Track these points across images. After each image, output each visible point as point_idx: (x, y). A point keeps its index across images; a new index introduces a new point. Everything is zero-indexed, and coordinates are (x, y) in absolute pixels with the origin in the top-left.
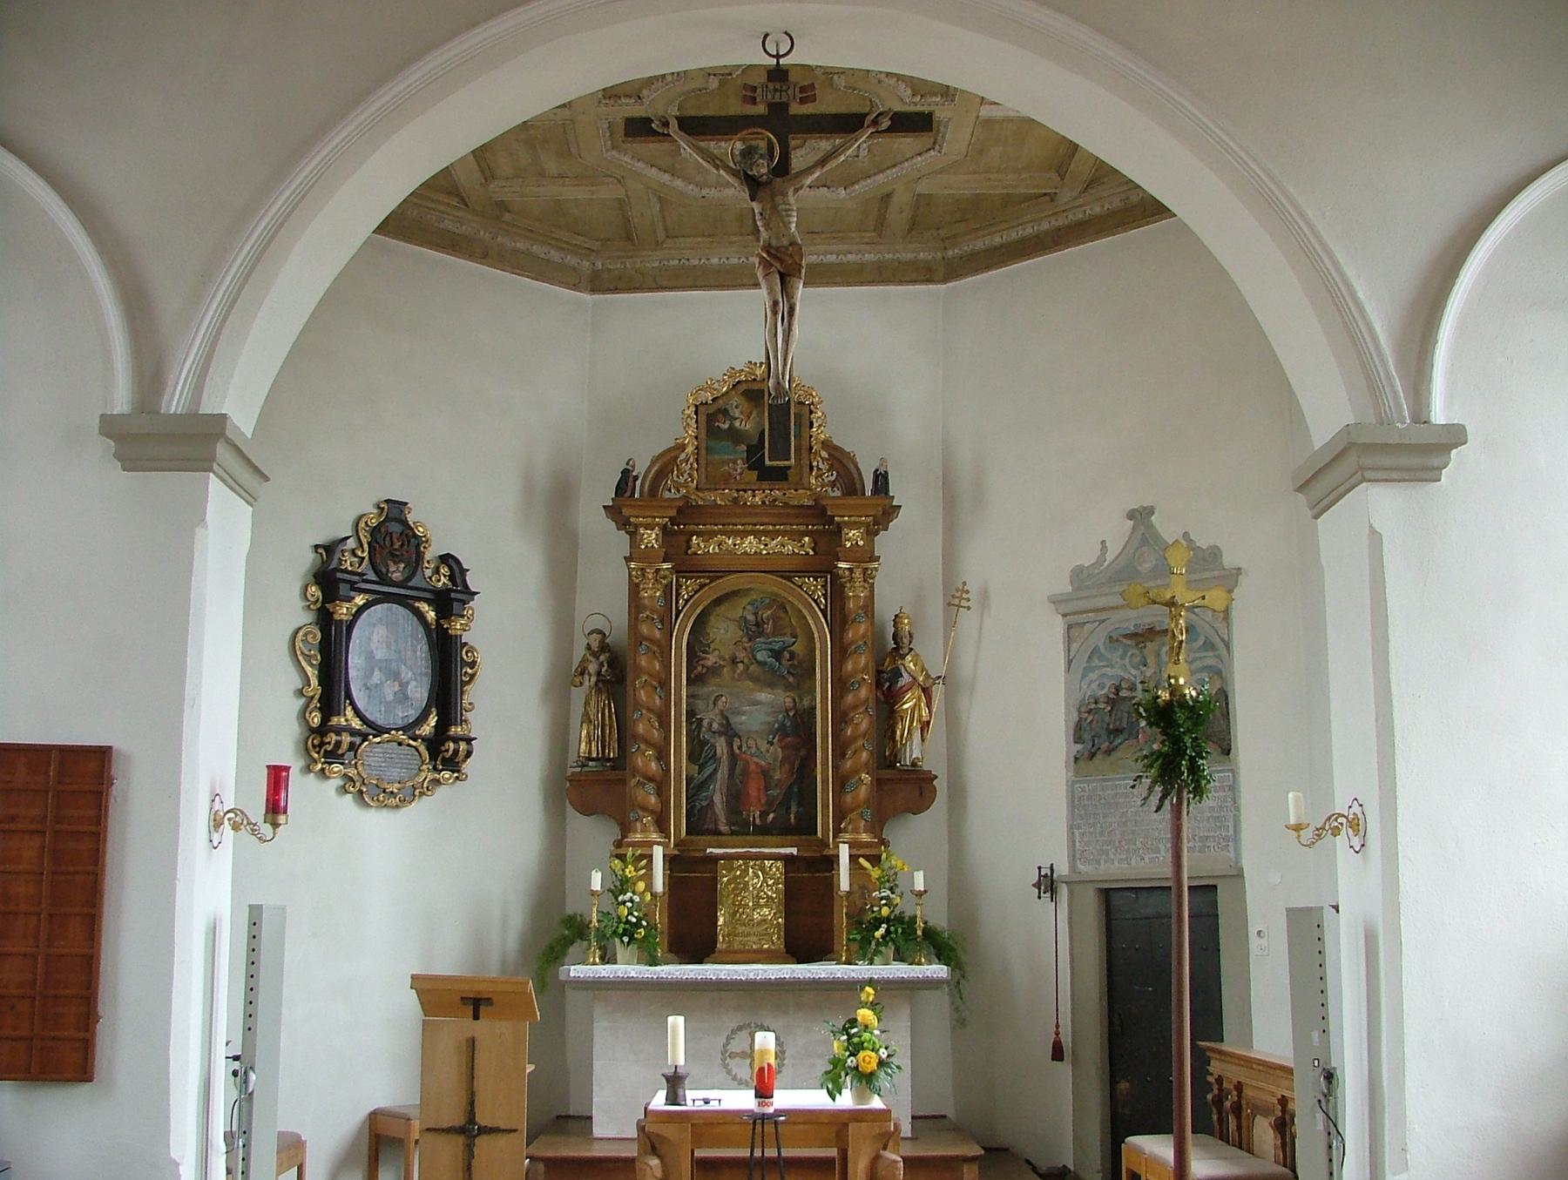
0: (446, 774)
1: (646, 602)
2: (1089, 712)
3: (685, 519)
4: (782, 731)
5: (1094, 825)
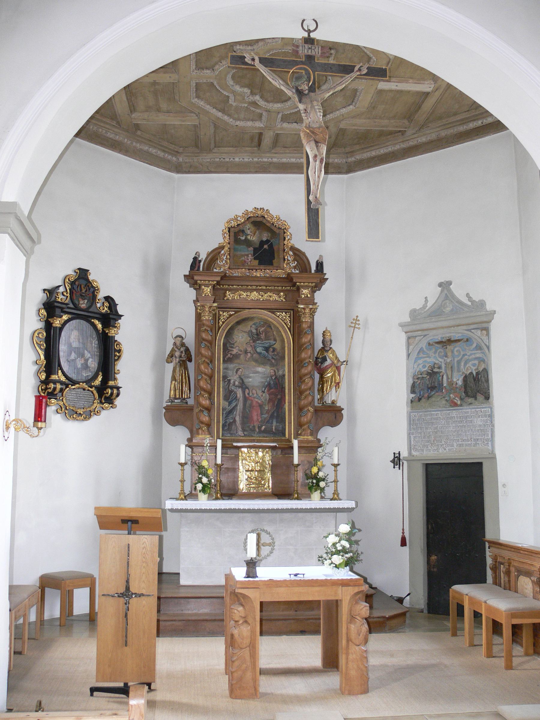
0: (106, 405)
1: (204, 322)
2: (418, 379)
3: (223, 284)
5: (421, 433)
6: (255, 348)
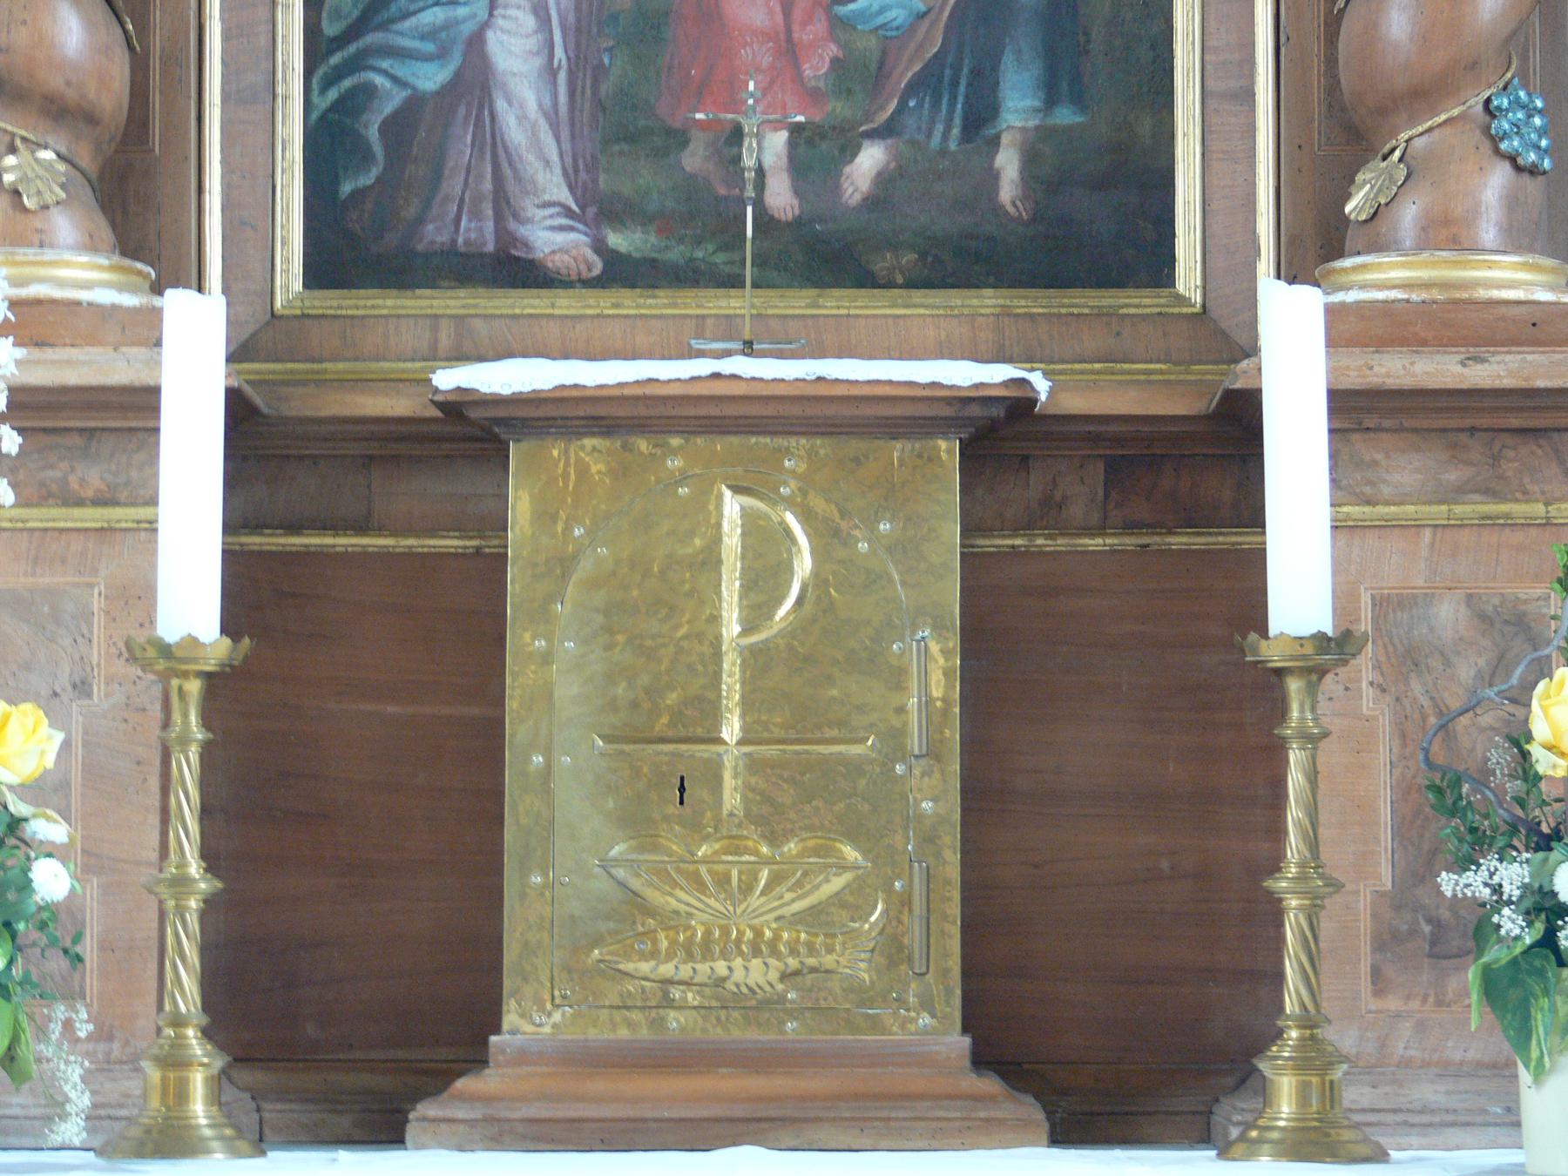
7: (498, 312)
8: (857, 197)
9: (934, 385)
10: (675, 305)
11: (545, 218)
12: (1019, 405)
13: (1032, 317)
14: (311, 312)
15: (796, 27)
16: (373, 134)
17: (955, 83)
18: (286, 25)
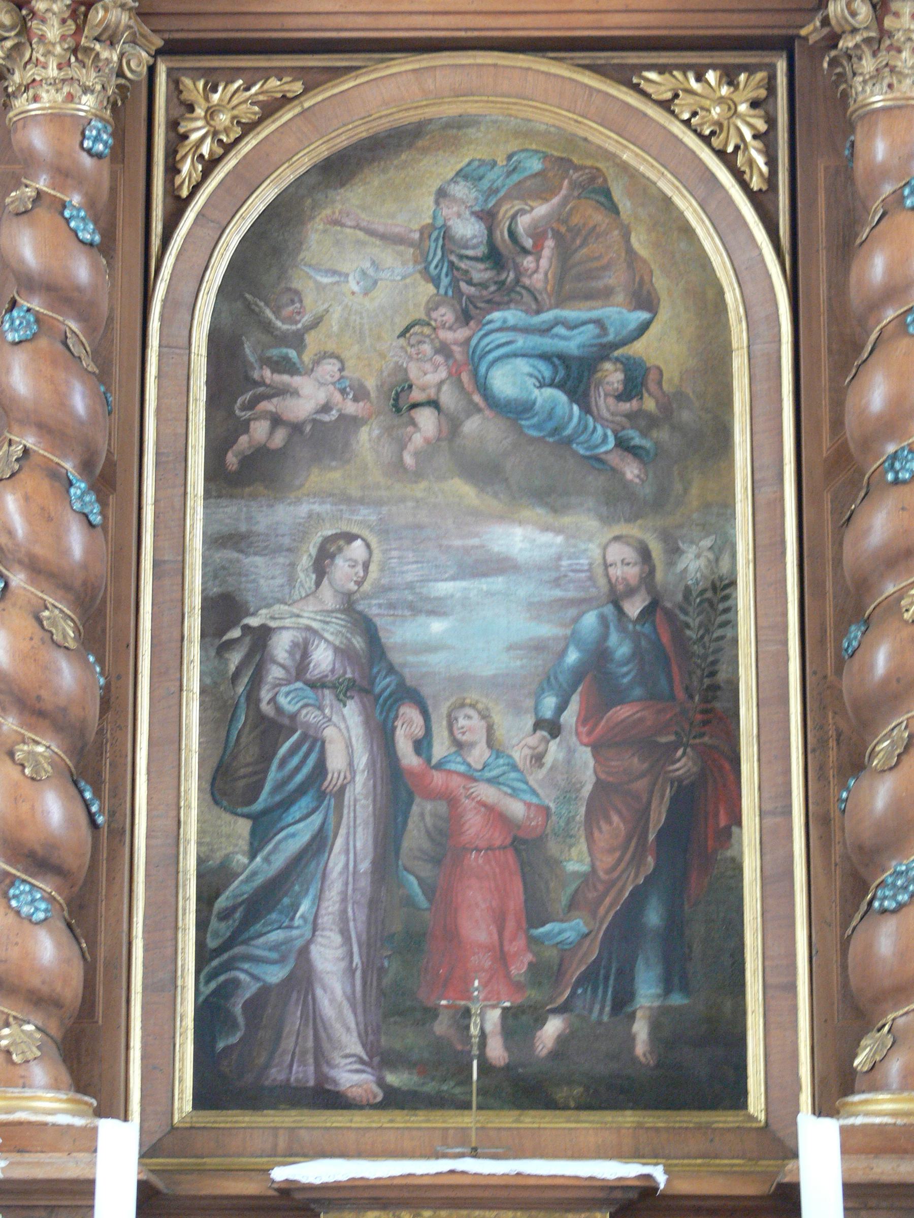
1: (38, 140)
4: (596, 675)
6: (471, 369)
7: (317, 1125)
8: (544, 1052)
9: (591, 1178)
10: (428, 1121)
11: (346, 1064)
12: (646, 1191)
13: (657, 1130)
14: (198, 1125)
15: (506, 943)
16: (238, 1010)
17: (607, 978)
18: (184, 942)
